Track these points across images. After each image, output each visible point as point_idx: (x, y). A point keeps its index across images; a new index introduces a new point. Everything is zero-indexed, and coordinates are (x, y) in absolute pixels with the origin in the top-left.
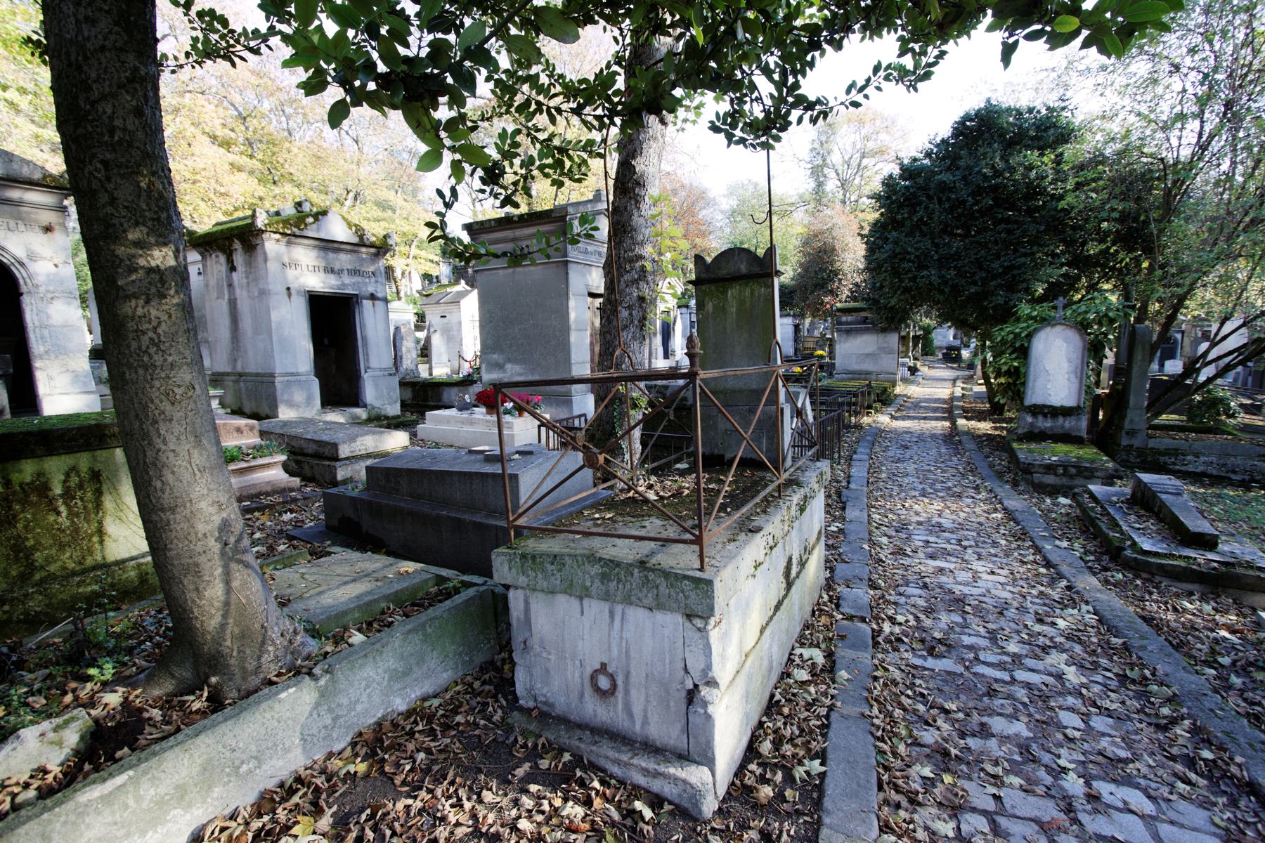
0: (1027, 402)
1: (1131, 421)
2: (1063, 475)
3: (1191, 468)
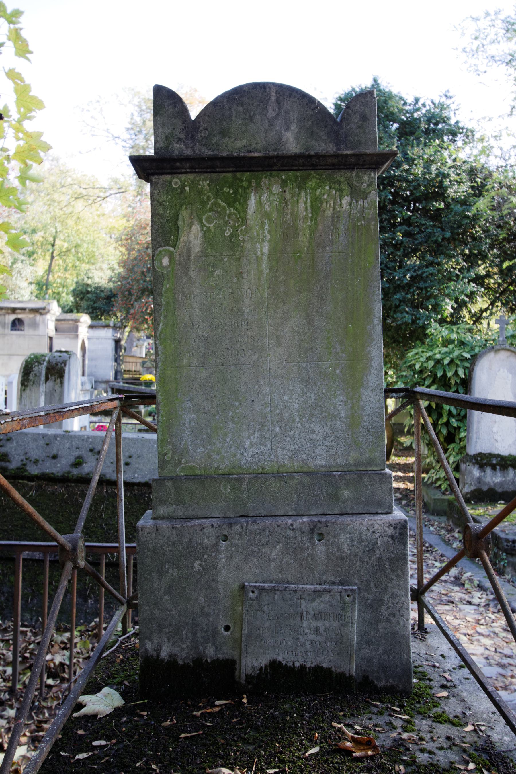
0: (473, 449)
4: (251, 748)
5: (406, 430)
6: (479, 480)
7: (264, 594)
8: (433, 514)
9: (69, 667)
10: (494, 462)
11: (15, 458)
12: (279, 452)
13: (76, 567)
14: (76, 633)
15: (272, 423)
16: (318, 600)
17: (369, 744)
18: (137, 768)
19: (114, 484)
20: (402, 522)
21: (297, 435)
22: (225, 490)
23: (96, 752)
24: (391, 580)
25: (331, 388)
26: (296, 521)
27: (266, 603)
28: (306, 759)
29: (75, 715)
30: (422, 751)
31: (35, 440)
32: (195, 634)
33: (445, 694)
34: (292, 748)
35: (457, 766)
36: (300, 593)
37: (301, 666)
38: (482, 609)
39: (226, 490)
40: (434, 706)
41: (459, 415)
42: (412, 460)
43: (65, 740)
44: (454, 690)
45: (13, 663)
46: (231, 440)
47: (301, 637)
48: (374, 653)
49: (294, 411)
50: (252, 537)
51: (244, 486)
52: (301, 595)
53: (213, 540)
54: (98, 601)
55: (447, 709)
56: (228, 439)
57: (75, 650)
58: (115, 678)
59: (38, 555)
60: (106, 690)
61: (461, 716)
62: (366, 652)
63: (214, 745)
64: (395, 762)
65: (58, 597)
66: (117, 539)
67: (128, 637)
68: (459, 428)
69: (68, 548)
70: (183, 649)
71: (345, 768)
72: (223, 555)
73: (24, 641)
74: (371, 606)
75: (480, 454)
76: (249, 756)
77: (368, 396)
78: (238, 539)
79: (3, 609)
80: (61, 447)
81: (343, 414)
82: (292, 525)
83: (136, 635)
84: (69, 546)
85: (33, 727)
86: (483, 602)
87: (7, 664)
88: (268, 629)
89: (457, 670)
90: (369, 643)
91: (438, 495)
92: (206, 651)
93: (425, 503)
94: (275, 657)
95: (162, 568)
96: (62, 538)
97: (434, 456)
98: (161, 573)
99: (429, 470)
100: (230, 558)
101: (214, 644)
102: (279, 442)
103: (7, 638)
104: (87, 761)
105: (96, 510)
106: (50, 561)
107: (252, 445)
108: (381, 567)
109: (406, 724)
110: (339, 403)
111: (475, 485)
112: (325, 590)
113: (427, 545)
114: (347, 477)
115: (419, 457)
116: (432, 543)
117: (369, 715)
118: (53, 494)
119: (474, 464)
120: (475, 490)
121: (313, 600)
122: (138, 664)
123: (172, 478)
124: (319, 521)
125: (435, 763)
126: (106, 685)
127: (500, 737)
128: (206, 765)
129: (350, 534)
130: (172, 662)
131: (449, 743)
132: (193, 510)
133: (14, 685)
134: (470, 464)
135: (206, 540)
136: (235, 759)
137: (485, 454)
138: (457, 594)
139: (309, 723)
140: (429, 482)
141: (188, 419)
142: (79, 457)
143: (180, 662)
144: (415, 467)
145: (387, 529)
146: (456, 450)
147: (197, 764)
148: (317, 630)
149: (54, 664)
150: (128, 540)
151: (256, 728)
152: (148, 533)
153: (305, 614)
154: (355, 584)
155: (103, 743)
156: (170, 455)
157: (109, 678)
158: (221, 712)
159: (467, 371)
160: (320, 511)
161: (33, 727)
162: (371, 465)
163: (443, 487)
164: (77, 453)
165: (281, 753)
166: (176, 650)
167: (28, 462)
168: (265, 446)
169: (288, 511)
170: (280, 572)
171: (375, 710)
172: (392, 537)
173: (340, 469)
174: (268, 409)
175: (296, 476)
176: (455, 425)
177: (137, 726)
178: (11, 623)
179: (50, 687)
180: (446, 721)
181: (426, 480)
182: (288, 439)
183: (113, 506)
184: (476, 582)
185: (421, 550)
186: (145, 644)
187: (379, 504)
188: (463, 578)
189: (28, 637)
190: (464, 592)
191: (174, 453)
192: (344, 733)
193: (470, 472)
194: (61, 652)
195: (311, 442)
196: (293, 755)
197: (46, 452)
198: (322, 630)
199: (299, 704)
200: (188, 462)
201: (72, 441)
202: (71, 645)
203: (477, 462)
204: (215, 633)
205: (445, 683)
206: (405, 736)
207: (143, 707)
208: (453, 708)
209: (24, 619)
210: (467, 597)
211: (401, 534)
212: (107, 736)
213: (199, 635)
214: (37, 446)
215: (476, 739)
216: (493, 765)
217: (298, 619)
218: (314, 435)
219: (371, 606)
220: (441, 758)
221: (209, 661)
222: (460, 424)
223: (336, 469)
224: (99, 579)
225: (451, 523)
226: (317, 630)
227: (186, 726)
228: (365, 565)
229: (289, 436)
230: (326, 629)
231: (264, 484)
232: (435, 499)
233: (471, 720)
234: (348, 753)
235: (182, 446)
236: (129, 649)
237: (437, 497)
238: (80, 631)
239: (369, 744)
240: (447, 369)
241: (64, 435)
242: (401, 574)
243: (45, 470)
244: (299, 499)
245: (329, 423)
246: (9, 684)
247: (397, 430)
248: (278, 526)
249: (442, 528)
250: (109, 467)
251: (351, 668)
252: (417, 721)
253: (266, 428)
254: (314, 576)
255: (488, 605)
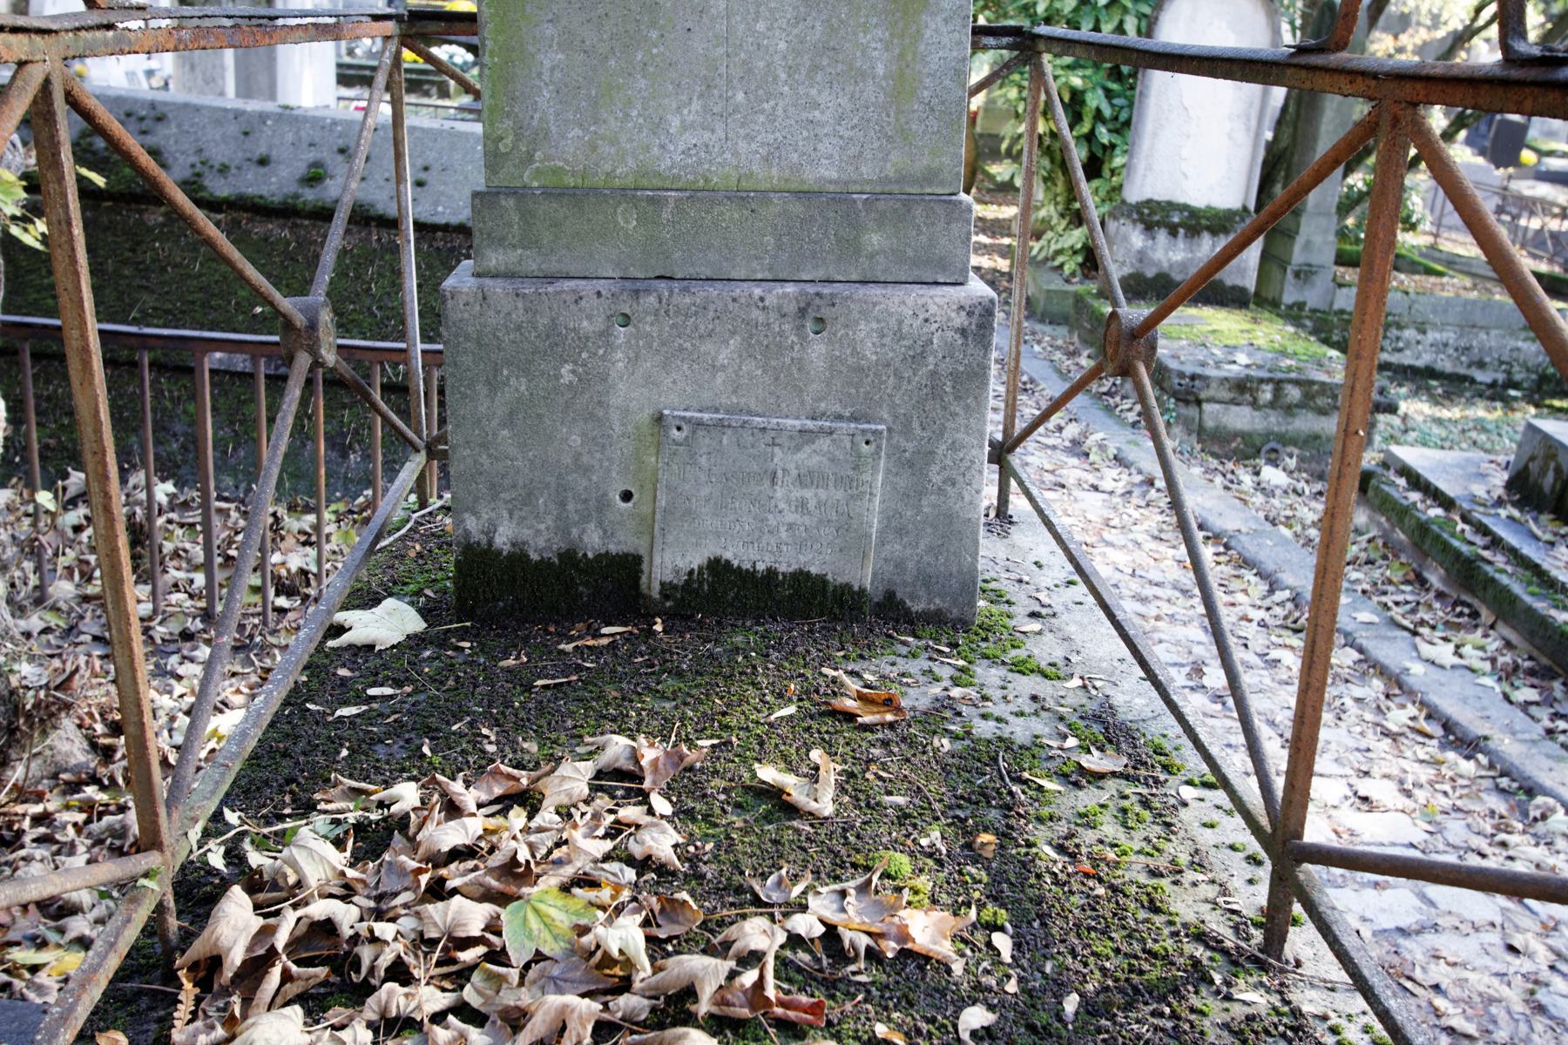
0: (1133, 195)
1: (1308, 245)
2: (1272, 405)
3: (1407, 359)
4: (668, 705)
5: (1004, 146)
6: (1142, 256)
7: (701, 433)
8: (1042, 321)
9: (318, 576)
10: (1176, 220)
11: (176, 159)
12: (742, 146)
13: (317, 363)
14: (328, 516)
15: (729, 81)
16: (807, 449)
17: (889, 703)
18: (454, 733)
19: (391, 224)
20: (986, 302)
21: (780, 112)
22: (627, 222)
23: (375, 706)
24: (954, 415)
25: (859, 9)
26: (770, 291)
27: (705, 450)
28: (771, 725)
29: (331, 643)
30: (984, 717)
31: (218, 123)
32: (563, 504)
33: (1035, 626)
34: (745, 707)
35: (1045, 741)
36: (773, 434)
37: (769, 570)
38: (1116, 500)
39: (628, 221)
40: (1013, 647)
41: (1116, 118)
42: (1009, 212)
43: (315, 685)
44: (1053, 620)
45: (207, 567)
46: (640, 115)
47: (770, 516)
48: (909, 551)
49: (777, 58)
50: (679, 320)
51: (666, 215)
52: (774, 438)
53: (600, 323)
54: (368, 457)
55: (1036, 651)
56: (634, 113)
57: (327, 547)
58: (405, 584)
59: (241, 362)
60: (389, 603)
61: (1061, 663)
62: (895, 548)
63: (598, 699)
64: (935, 733)
65: (283, 418)
66: (402, 336)
67: (430, 513)
68: (1113, 146)
69: (298, 324)
70: (538, 531)
71: (842, 741)
72: (620, 355)
73: (225, 526)
74: (911, 464)
75: (1149, 201)
76: (665, 719)
77: (936, 31)
78: (652, 324)
79: (179, 467)
80: (276, 141)
81: (880, 70)
82: (762, 299)
83: (446, 509)
84: (300, 320)
85: (254, 679)
86: (1120, 488)
87: (196, 568)
88: (707, 501)
89: (1062, 589)
90: (901, 532)
91: (1057, 284)
92: (585, 538)
93: (1028, 299)
94: (718, 552)
95: (495, 376)
96: (286, 304)
97: (1056, 204)
98: (494, 386)
99: (1044, 232)
100: (634, 360)
101: (600, 524)
102: (743, 125)
103: (191, 520)
104: (358, 720)
105: (357, 277)
106: (267, 377)
107: (684, 128)
108: (935, 391)
109: (958, 674)
110: (873, 45)
111: (1132, 265)
112: (821, 430)
113: (1025, 378)
114: (881, 205)
115: (1027, 210)
116: (1035, 376)
117: (892, 658)
118: (266, 240)
119: (1134, 222)
120: (1131, 276)
121: (798, 448)
122: (450, 561)
123: (513, 192)
124: (818, 294)
125: (1006, 735)
126: (391, 595)
127: (1128, 698)
128: (582, 731)
129: (878, 321)
130: (518, 558)
131: (1035, 706)
132: (559, 261)
133: (211, 604)
134: (1128, 222)
135: (585, 323)
136: (638, 723)
137: (1159, 203)
138: (1073, 470)
139: (779, 668)
140: (1040, 257)
141: (547, 64)
142: (316, 164)
143: (534, 557)
144: (1015, 229)
145: (953, 315)
146: (1102, 193)
147: (566, 729)
148: (802, 505)
149: (288, 571)
150: (426, 338)
151: (680, 674)
152: (466, 304)
153: (780, 473)
154: (882, 421)
155: (388, 691)
156: (509, 140)
157: (395, 583)
158: (613, 646)
159: (1144, 24)
160: (821, 274)
161: (254, 679)
162: (930, 184)
163: (1066, 267)
164: (311, 156)
165: (724, 714)
166: (526, 534)
167: (206, 169)
168: (713, 131)
169: (754, 272)
170: (735, 392)
171: (904, 650)
172: (963, 332)
173: (868, 189)
174: (721, 50)
175: (775, 197)
176: (1105, 141)
177: (452, 665)
178: (195, 494)
179: (282, 611)
180: (1032, 671)
181: (1034, 252)
182: (762, 118)
183: (393, 271)
184: (1112, 451)
185: (1015, 385)
186: (463, 521)
187: (942, 264)
188: (1089, 442)
189: (232, 520)
190: (1087, 467)
191: (518, 137)
192: (842, 685)
193: (1126, 239)
194: (301, 549)
195: (810, 127)
196: (747, 719)
197: (245, 151)
198: (812, 505)
199: (762, 637)
200: (547, 158)
201: (299, 130)
202: (319, 536)
203: (1142, 220)
204: (603, 504)
205: (1038, 608)
206: (956, 692)
207: (463, 634)
208: (1045, 650)
209: (223, 485)
210: (1091, 478)
211: (981, 326)
212: (394, 679)
213: (570, 507)
214: (224, 136)
215: (1084, 701)
216: (1110, 742)
217: (767, 483)
218: (817, 113)
219: (911, 464)
220: (1018, 729)
221: (590, 555)
222: (1116, 139)
223: (859, 189)
224: (367, 397)
225: (1076, 339)
226: (802, 505)
227: (545, 667)
228: (905, 386)
229: (763, 111)
230: (819, 504)
231: (707, 212)
232: (1049, 291)
233: (1078, 671)
234: (850, 717)
235: (535, 123)
236: (433, 534)
237: (1053, 287)
238: (335, 512)
239: (889, 703)
240: (1103, 16)
241: (281, 115)
242: (973, 405)
243: (243, 190)
244: (779, 247)
245: (850, 88)
246: (202, 604)
247: (985, 148)
248: (734, 300)
249: (1058, 348)
250: (381, 188)
251: (864, 576)
252: (979, 670)
253: (716, 92)
254: (802, 403)
255: (1130, 493)
